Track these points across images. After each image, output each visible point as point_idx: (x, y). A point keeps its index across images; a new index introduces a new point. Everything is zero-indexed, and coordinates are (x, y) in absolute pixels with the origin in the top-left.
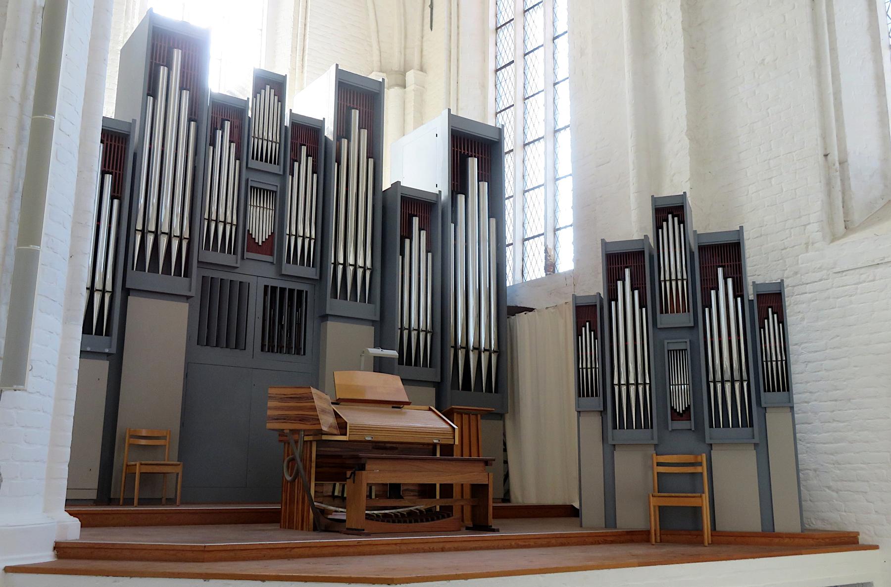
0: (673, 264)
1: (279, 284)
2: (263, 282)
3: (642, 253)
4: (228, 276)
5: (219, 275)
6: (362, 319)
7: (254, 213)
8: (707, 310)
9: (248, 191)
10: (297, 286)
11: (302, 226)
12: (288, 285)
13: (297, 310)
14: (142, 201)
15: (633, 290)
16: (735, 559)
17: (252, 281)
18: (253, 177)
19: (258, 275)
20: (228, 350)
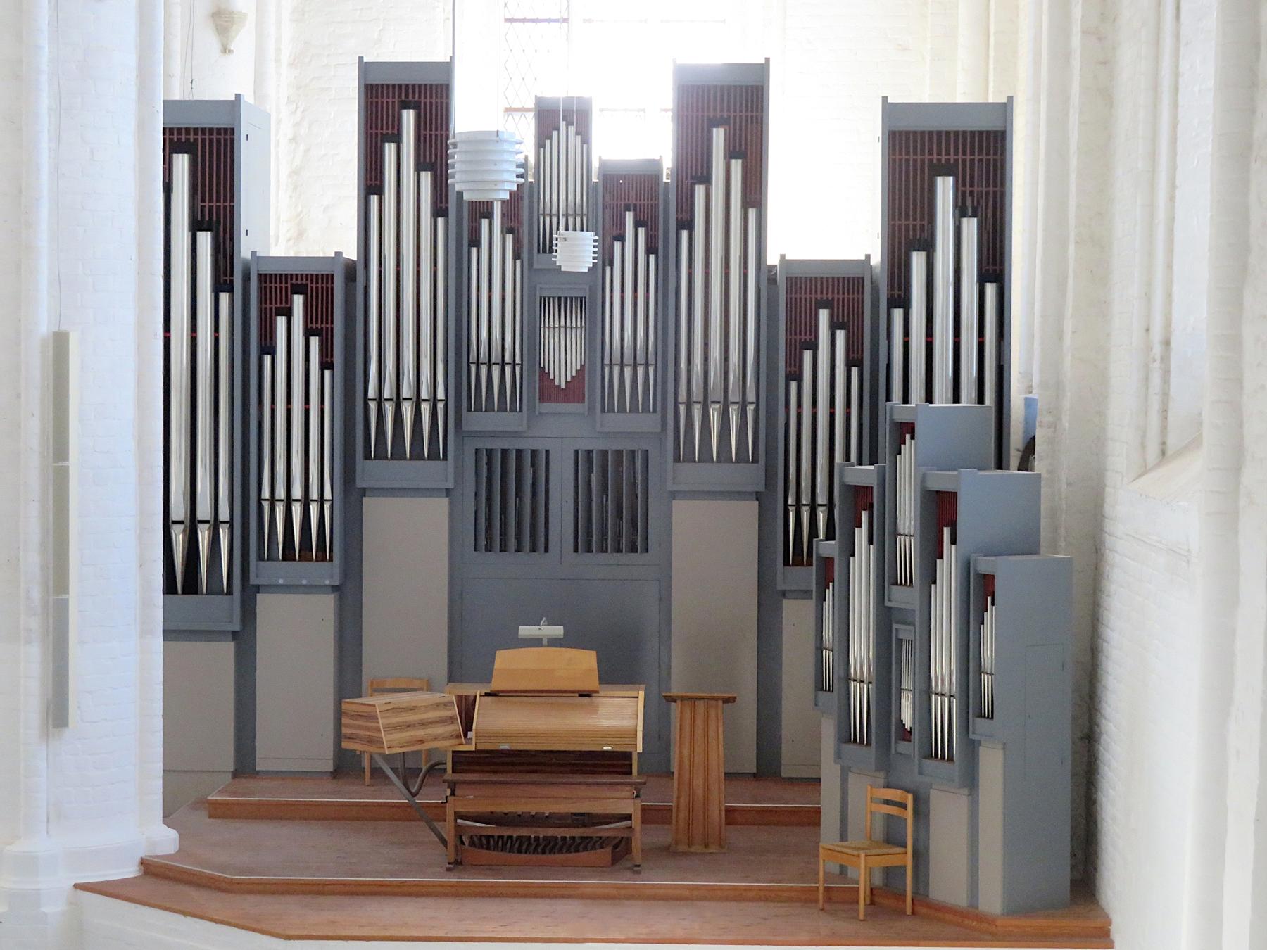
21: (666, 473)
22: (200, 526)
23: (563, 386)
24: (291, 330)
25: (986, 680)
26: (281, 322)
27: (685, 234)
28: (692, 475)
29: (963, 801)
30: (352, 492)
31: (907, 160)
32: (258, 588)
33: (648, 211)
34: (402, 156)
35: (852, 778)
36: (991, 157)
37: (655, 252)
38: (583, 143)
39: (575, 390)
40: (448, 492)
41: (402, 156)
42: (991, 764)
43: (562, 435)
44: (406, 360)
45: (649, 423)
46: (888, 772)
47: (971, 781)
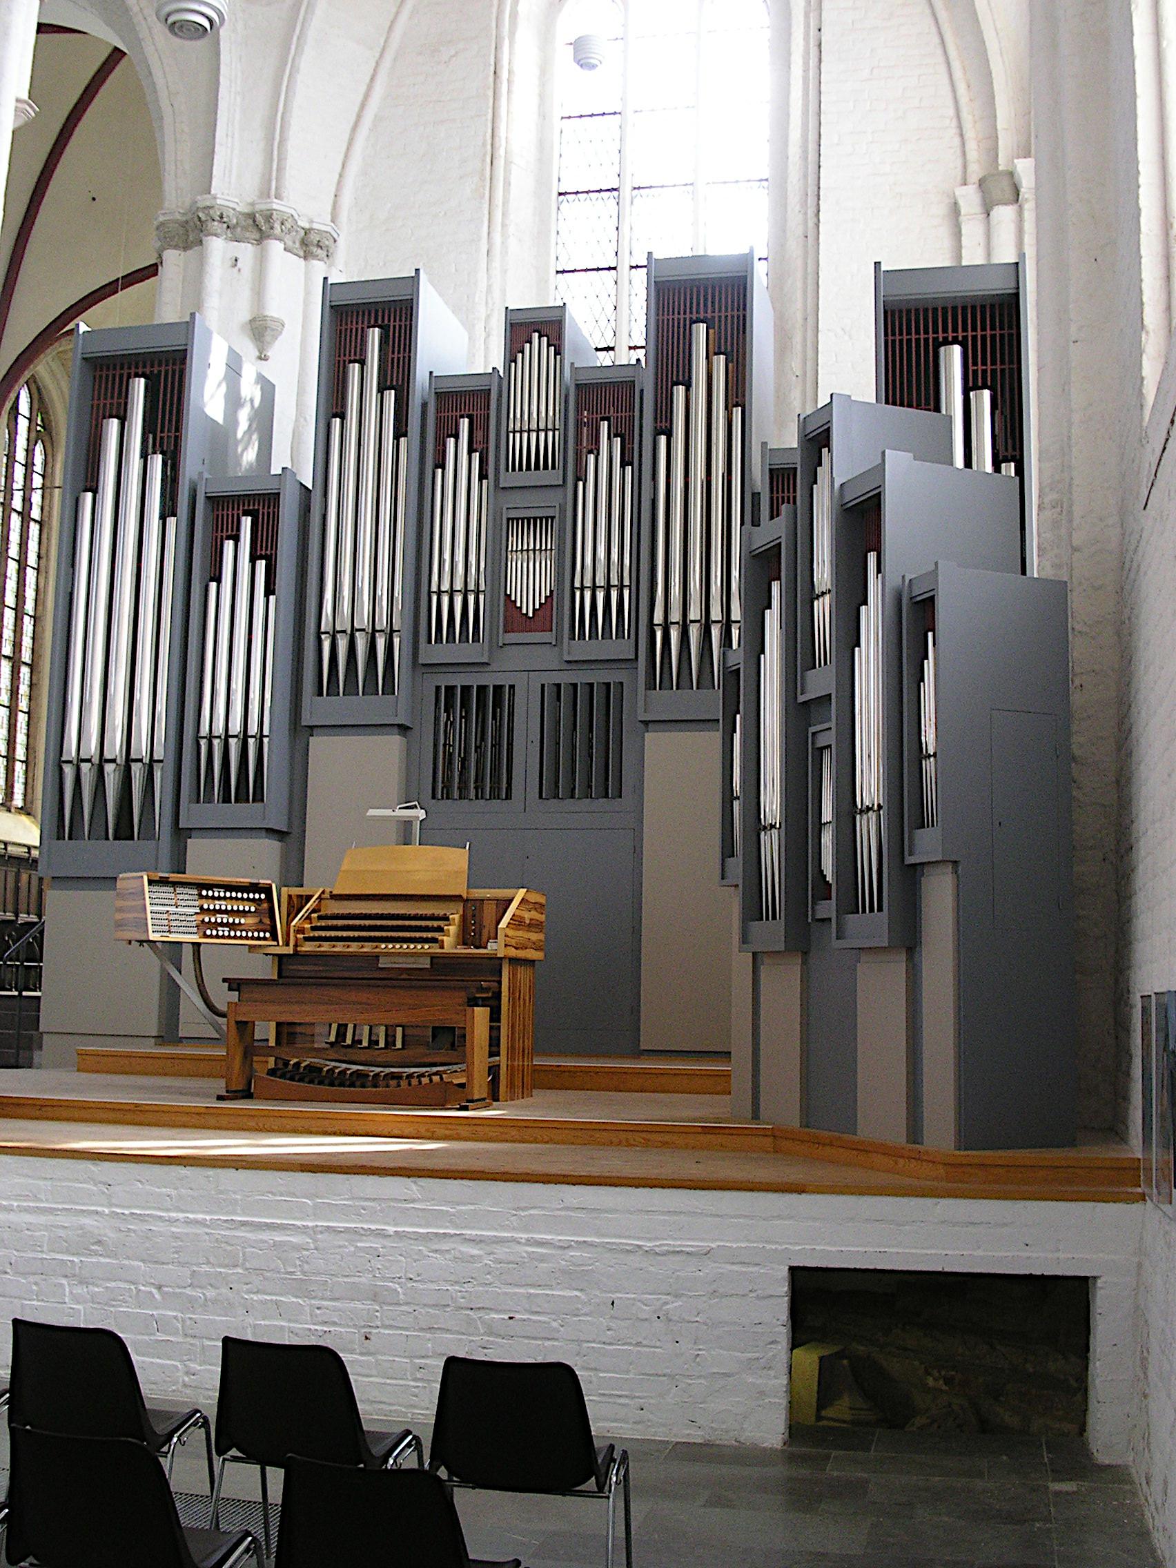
0: (534, 409)
1: (565, 678)
2: (536, 681)
3: (273, 498)
4: (474, 680)
5: (458, 680)
6: (709, 720)
7: (517, 564)
8: (581, 484)
9: (504, 526)
10: (597, 677)
11: (601, 549)
12: (581, 677)
13: (494, 718)
14: (735, 573)
15: (253, 560)
16: (875, 1271)
17: (520, 681)
18: (517, 499)
19: (528, 670)
20: (482, 802)
21: (642, 702)
22: (133, 765)
23: (531, 615)
24: (237, 556)
25: (929, 766)
26: (229, 545)
27: (663, 439)
28: (665, 703)
29: (897, 968)
30: (300, 731)
31: (909, 341)
32: (189, 832)
33: (610, 407)
34: (363, 380)
35: (764, 971)
36: (1006, 332)
37: (632, 464)
38: (556, 354)
39: (544, 615)
40: (403, 729)
41: (363, 380)
42: (940, 897)
43: (528, 670)
44: (361, 586)
45: (621, 648)
46: (805, 953)
47: (909, 938)
